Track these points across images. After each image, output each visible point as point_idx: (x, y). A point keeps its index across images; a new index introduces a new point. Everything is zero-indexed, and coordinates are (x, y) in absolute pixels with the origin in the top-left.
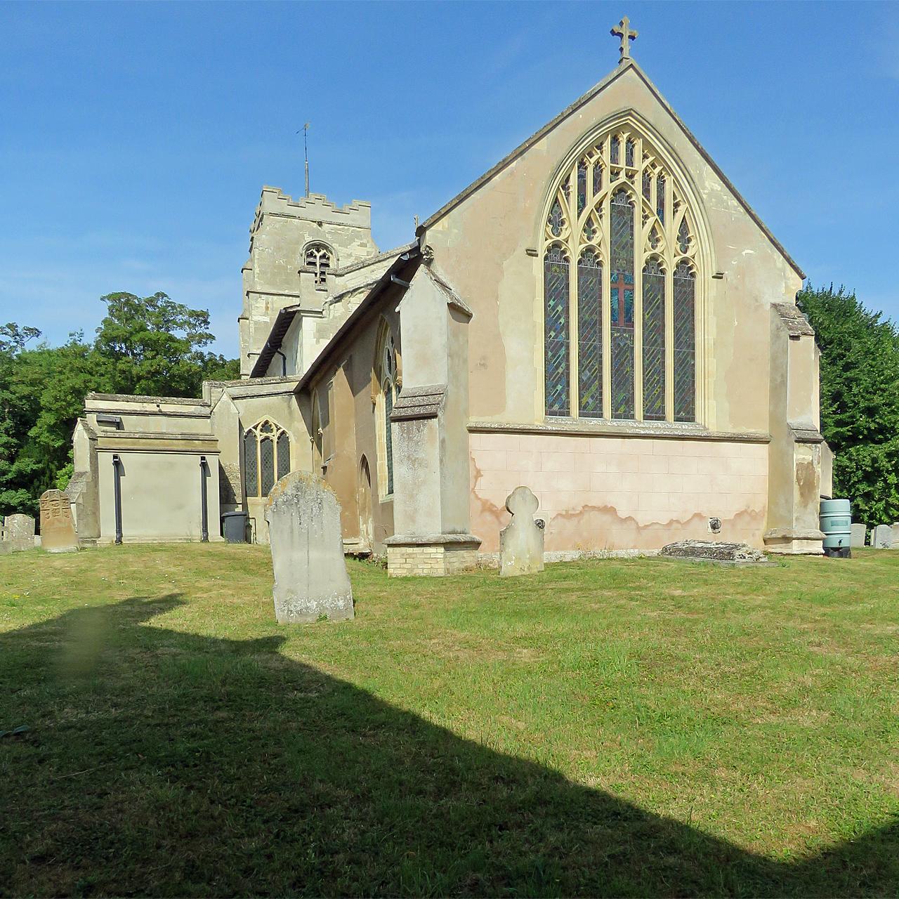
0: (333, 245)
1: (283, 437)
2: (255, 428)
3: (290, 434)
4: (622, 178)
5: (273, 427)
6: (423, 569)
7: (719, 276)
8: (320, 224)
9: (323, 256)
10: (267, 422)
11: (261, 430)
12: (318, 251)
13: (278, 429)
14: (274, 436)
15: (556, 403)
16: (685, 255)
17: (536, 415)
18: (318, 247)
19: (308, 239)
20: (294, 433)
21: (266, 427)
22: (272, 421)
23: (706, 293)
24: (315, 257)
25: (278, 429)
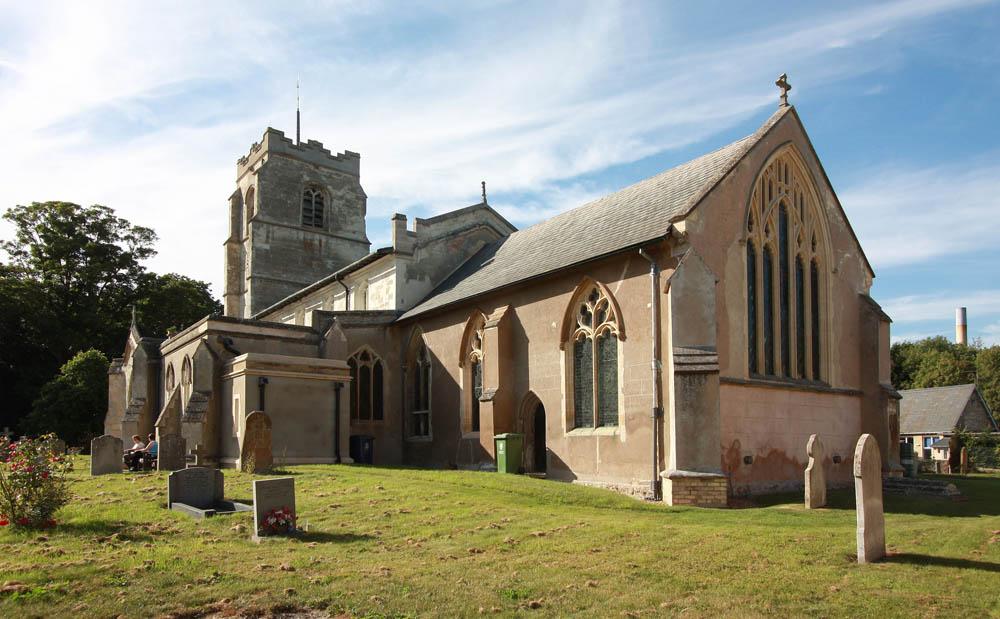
1: (378, 367)
2: (356, 355)
5: (371, 356)
7: (835, 272)
9: (318, 196)
12: (314, 191)
15: (753, 368)
17: (745, 375)
21: (365, 356)
22: (370, 350)
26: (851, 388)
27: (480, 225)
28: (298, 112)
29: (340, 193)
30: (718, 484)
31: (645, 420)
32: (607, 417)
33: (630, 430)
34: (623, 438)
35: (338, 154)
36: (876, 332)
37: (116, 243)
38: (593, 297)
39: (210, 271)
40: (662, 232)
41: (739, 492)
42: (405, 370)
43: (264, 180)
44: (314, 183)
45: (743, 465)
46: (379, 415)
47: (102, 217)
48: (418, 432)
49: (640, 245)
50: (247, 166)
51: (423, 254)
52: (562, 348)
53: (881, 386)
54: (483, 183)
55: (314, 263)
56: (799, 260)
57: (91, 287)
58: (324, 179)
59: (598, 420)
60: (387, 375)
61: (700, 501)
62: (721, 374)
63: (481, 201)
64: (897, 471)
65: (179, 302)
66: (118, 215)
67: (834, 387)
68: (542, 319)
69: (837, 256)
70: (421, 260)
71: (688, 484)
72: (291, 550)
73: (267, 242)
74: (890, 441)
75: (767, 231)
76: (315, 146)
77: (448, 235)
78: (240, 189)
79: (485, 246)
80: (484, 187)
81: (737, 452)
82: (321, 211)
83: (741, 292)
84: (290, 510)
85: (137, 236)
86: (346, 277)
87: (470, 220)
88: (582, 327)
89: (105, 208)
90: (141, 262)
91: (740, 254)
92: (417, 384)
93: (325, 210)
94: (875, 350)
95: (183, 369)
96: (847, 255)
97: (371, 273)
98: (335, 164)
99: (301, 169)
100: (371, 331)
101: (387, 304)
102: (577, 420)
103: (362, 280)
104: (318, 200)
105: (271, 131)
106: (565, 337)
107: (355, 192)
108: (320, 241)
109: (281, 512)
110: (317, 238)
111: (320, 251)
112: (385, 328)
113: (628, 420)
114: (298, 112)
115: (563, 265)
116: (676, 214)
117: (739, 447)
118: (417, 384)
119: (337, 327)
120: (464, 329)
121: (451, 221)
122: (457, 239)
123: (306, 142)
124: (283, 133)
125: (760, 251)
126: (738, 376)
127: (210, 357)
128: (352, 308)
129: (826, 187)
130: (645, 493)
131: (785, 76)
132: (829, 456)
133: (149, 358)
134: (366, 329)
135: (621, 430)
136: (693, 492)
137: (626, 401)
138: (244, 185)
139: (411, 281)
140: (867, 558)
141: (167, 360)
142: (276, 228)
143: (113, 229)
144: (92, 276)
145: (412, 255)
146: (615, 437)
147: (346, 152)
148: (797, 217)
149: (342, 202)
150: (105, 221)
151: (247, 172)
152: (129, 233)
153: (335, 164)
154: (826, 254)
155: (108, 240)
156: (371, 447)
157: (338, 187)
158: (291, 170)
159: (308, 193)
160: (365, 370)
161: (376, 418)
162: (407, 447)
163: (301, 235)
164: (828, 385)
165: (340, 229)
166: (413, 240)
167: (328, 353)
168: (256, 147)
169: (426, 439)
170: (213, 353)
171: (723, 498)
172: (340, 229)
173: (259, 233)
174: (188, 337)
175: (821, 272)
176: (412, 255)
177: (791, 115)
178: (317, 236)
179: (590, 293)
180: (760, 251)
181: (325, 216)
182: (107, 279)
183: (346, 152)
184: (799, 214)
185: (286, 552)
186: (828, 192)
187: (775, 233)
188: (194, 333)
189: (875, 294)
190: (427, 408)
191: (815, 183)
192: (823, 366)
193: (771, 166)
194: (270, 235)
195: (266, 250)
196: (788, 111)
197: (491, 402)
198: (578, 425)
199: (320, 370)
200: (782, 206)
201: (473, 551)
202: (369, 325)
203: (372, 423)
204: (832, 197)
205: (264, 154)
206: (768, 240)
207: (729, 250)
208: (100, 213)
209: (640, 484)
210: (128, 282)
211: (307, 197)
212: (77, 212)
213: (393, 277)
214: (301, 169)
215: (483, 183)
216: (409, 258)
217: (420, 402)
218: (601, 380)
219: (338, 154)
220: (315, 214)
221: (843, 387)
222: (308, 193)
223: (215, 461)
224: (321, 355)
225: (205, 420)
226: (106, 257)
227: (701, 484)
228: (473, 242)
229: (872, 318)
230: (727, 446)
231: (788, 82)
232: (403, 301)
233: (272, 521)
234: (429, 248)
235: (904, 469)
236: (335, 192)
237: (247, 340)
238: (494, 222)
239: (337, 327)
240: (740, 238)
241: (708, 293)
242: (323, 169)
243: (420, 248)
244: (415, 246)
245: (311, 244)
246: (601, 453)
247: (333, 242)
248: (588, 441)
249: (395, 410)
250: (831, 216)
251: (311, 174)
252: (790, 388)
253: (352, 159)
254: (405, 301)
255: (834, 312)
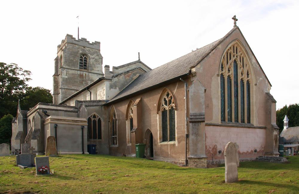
0: (89, 54)
1: (99, 120)
2: (91, 116)
3: (102, 119)
4: (235, 57)
5: (96, 116)
6: (200, 165)
7: (256, 85)
8: (84, 47)
9: (85, 58)
10: (94, 115)
11: (93, 117)
12: (83, 56)
13: (98, 117)
14: (97, 120)
15: (223, 119)
16: (222, 72)
17: (219, 122)
18: (84, 55)
19: (81, 52)
20: (103, 118)
21: (94, 116)
22: (96, 114)
23: (253, 89)
24: (82, 58)
25: (98, 117)
26: (262, 126)
27: (137, 68)
28: (78, 28)
29: (93, 57)
30: (204, 160)
31: (183, 138)
32: (172, 138)
33: (179, 142)
34: (177, 145)
35: (92, 42)
36: (271, 106)
37: (18, 76)
38: (168, 95)
39: (48, 85)
40: (187, 72)
41: (216, 163)
42: (109, 121)
43: (65, 53)
44: (83, 53)
45: (218, 153)
46: (100, 137)
47: (14, 67)
48: (114, 144)
49: (180, 77)
50: (60, 48)
51: (116, 79)
52: (158, 114)
53: (272, 125)
54: (139, 53)
55: (84, 82)
56: (242, 80)
57: (10, 92)
58: (87, 52)
59: (170, 138)
60: (103, 123)
61: (198, 166)
62: (206, 122)
63: (137, 59)
64: (277, 154)
65: (39, 96)
66: (19, 66)
67: (255, 125)
68: (151, 102)
69: (257, 80)
70: (115, 82)
71: (194, 160)
72: (43, 178)
73: (67, 75)
74: (274, 144)
75: (229, 71)
76: (84, 40)
77: (125, 72)
78: (58, 56)
79: (140, 76)
80: (139, 54)
81: (216, 149)
82: (86, 63)
83: (218, 93)
84: (48, 167)
85: (25, 73)
86: (90, 88)
87: (134, 67)
88: (165, 106)
89: (15, 64)
90: (26, 83)
91: (217, 79)
92: (113, 126)
93: (87, 63)
94: (270, 112)
95: (33, 121)
96: (261, 79)
97: (98, 85)
98: (91, 46)
99: (79, 48)
100: (97, 107)
101: (103, 97)
102: (164, 139)
103: (94, 89)
104: (85, 59)
105: (68, 35)
106: (159, 109)
107: (98, 56)
108: (86, 74)
109: (44, 167)
110: (84, 73)
111: (86, 78)
112: (102, 106)
113: (178, 139)
114: (78, 28)
115: (157, 84)
116: (192, 66)
117: (217, 147)
118: (113, 126)
119: (83, 106)
120: (127, 106)
121: (126, 67)
122: (129, 74)
123: (81, 39)
124: (72, 36)
125: (226, 78)
126: (216, 123)
127: (39, 117)
128: (92, 99)
129: (252, 55)
130: (183, 164)
131: (235, 16)
132: (253, 150)
133: (23, 117)
134: (95, 107)
135: (176, 142)
136: (195, 163)
137: (178, 132)
138: (59, 54)
139: (111, 89)
140: (227, 181)
141: (28, 118)
142: (69, 70)
143: (17, 71)
144: (10, 88)
145: (111, 80)
146: (174, 145)
147: (95, 41)
148: (241, 65)
149: (94, 60)
150: (14, 69)
151: (60, 50)
152: (23, 73)
153: (91, 46)
154: (252, 78)
155: (16, 75)
156: (95, 148)
157: (92, 54)
158: (75, 49)
159: (81, 57)
160: (95, 121)
161: (98, 139)
162: (110, 149)
163: (79, 72)
164: (253, 125)
165: (93, 70)
166: (112, 75)
167: (80, 116)
168: (63, 41)
169: (117, 146)
170: (40, 115)
171: (206, 165)
172: (93, 70)
173: (64, 72)
174: (34, 110)
175: (251, 85)
176: (111, 80)
177: (237, 30)
178: (85, 73)
179: (167, 93)
180: (226, 78)
181: (87, 65)
182: (16, 89)
183: (95, 41)
184: (242, 64)
185: (41, 179)
186: (253, 56)
187: (232, 72)
188: (35, 109)
189: (272, 92)
190: (116, 135)
191: (247, 53)
192: (251, 118)
193: (230, 48)
194: (68, 73)
195: (66, 78)
196: (236, 28)
197: (134, 133)
198: (164, 141)
199: (77, 121)
200: (235, 61)
201: (99, 180)
202: (96, 106)
203: (97, 140)
204: (255, 59)
205: (65, 44)
206: (230, 74)
207: (213, 78)
208: (13, 66)
209: (182, 161)
210: (22, 90)
211: (81, 59)
212: (5, 66)
213: (105, 88)
214: (79, 48)
215: (139, 53)
216: (111, 81)
217: (114, 133)
218: (171, 124)
219: (92, 42)
220: (84, 64)
221: (258, 126)
222: (81, 57)
223: (42, 153)
224: (78, 116)
225: (38, 139)
226: (15, 82)
227: (198, 160)
228: (135, 75)
229: (270, 100)
230: (212, 147)
231: (237, 18)
232: (108, 97)
233: (41, 170)
234: (118, 77)
235: (279, 154)
236: (91, 56)
237: (52, 111)
238: (143, 67)
239: (83, 106)
240: (217, 74)
241: (202, 93)
242: (87, 48)
243: (115, 77)
244: (113, 77)
245: (82, 76)
246: (170, 150)
247: (90, 74)
248: (166, 146)
249: (100, 136)
250: (254, 65)
251: (82, 50)
252: (237, 127)
253: (97, 44)
254: (109, 97)
255: (256, 100)
